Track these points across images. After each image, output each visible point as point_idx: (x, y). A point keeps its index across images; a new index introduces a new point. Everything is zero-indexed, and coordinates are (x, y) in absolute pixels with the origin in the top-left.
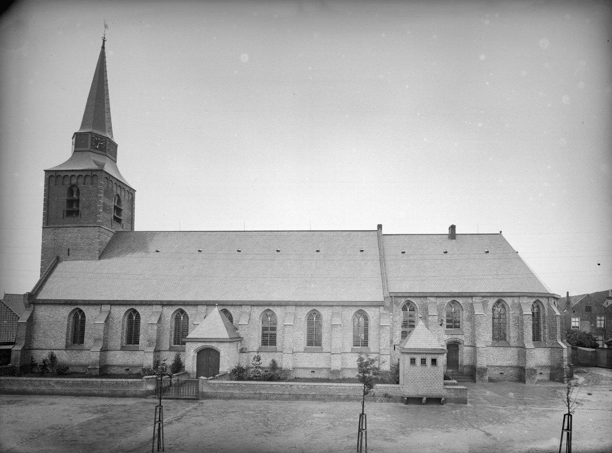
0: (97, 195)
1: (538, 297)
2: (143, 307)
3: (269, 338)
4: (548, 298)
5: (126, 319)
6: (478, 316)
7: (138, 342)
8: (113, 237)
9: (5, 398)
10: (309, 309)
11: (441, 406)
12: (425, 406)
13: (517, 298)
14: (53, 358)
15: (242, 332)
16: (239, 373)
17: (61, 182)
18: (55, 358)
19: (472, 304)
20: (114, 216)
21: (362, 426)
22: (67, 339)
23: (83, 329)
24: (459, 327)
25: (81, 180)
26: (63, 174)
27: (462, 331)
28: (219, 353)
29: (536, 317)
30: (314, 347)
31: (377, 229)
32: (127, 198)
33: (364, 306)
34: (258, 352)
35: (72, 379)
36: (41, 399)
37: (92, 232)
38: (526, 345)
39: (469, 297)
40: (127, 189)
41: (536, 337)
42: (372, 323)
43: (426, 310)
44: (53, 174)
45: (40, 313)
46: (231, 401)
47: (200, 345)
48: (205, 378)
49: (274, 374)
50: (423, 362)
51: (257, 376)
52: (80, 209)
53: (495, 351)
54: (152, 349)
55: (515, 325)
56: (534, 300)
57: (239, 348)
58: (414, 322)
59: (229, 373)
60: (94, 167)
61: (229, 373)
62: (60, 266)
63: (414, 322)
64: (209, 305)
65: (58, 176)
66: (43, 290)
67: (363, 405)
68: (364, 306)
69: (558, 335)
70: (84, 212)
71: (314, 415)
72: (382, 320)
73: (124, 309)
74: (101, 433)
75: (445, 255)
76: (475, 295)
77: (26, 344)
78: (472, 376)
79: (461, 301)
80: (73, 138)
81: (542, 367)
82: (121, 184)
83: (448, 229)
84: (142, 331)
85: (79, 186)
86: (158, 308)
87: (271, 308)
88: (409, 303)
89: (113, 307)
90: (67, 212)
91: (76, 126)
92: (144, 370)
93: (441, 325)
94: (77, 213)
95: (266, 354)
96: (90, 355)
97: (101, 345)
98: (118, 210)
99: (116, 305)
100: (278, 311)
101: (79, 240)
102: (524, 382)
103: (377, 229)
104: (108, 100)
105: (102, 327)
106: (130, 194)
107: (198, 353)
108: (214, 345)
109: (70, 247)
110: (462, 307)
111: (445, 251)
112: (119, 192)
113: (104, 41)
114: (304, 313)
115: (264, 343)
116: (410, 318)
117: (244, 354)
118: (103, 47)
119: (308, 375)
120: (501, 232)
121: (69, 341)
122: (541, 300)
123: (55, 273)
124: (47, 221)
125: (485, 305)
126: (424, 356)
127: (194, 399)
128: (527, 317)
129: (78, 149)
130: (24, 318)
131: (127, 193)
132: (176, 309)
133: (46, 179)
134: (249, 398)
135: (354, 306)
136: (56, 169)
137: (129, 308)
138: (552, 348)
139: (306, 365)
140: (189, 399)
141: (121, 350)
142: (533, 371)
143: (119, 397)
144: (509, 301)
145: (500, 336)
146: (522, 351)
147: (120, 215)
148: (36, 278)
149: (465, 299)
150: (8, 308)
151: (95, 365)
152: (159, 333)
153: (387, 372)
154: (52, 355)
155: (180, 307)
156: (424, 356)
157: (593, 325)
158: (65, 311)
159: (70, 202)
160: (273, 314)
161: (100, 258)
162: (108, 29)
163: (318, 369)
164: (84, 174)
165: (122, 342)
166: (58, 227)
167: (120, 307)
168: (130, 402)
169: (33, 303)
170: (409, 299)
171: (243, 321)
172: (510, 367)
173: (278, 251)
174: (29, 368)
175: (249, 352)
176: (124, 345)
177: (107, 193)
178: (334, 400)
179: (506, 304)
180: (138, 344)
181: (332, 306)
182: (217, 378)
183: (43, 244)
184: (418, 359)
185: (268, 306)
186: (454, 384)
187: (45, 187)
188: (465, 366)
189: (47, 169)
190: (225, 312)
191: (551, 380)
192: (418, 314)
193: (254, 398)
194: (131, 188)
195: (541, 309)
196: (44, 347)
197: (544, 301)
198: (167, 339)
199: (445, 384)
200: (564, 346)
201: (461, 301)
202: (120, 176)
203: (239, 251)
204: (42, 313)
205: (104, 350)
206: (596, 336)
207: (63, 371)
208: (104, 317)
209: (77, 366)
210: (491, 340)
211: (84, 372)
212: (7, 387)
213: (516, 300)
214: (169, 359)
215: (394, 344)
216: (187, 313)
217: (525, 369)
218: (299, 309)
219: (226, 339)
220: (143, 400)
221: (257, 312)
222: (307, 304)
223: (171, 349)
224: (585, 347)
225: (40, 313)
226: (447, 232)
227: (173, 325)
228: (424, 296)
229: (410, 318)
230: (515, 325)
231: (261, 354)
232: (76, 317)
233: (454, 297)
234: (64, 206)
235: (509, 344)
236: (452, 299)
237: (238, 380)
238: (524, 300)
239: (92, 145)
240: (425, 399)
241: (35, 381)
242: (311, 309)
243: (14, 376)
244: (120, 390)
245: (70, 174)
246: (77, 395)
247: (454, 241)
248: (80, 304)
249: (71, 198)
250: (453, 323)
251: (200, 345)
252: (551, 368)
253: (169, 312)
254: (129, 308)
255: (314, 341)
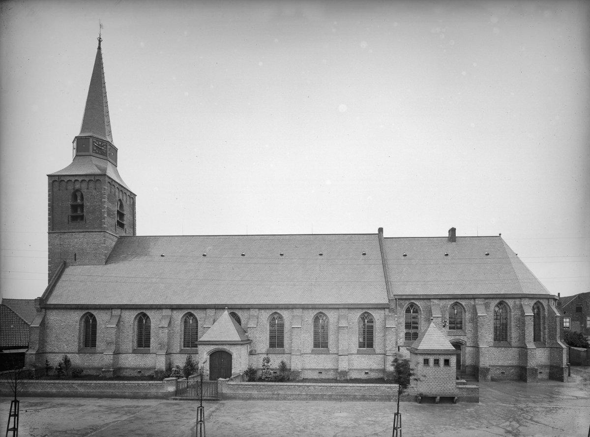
0: (101, 200)
1: (539, 298)
2: (153, 311)
3: (277, 341)
4: (548, 299)
5: (136, 323)
6: (481, 318)
7: (149, 345)
8: (118, 241)
9: (2, 398)
10: (316, 312)
11: (454, 405)
12: (438, 405)
13: (519, 300)
14: (67, 361)
15: (250, 334)
16: (251, 375)
17: (64, 187)
18: (69, 361)
19: (474, 306)
20: (118, 221)
21: (397, 424)
22: (79, 343)
23: (148, 334)
24: (461, 328)
25: (84, 185)
26: (66, 179)
27: (465, 333)
28: (231, 355)
29: (537, 317)
30: (321, 349)
31: (377, 233)
32: (128, 203)
33: (369, 308)
34: (267, 354)
35: (95, 382)
36: (66, 401)
37: (97, 237)
38: (527, 345)
39: (471, 299)
40: (128, 194)
41: (537, 339)
42: (377, 326)
43: (430, 311)
44: (56, 179)
45: (52, 318)
46: (251, 402)
47: (212, 348)
48: (224, 379)
49: (284, 375)
50: (437, 362)
51: (268, 378)
52: (85, 214)
53: (496, 352)
54: (164, 352)
55: (516, 326)
56: (535, 301)
57: (249, 350)
58: (417, 323)
59: (241, 374)
60: (97, 171)
61: (241, 374)
62: (68, 271)
63: (417, 323)
64: (218, 309)
65: (62, 180)
66: (53, 294)
67: (398, 405)
68: (369, 308)
69: (558, 335)
70: (89, 217)
71: (336, 415)
72: (387, 322)
73: (134, 314)
74: (139, 433)
75: (445, 257)
76: (478, 297)
77: (39, 347)
78: (474, 375)
79: (463, 303)
80: (73, 142)
81: (542, 366)
82: (126, 191)
83: (448, 231)
84: (152, 334)
85: (82, 191)
86: (167, 312)
87: (278, 311)
88: (412, 305)
89: (124, 311)
90: (72, 217)
91: (77, 132)
92: (157, 372)
93: (444, 326)
94: (82, 218)
95: (274, 355)
96: (102, 358)
97: (113, 347)
98: (121, 215)
99: (126, 309)
100: (285, 314)
101: (85, 245)
102: (525, 381)
103: (377, 233)
104: (107, 103)
105: (114, 331)
106: (131, 199)
107: (211, 356)
108: (227, 348)
109: (77, 252)
110: (464, 308)
111: (446, 253)
112: (121, 198)
113: (100, 41)
114: (310, 315)
115: (272, 345)
116: (413, 320)
117: (254, 356)
118: (99, 48)
119: (315, 376)
120: (500, 234)
121: (81, 344)
122: (541, 301)
123: (63, 278)
124: (53, 226)
125: (487, 306)
126: (437, 357)
127: (214, 400)
128: (529, 318)
129: (80, 154)
130: (36, 323)
131: (128, 198)
132: (84, 313)
133: (49, 184)
134: (267, 399)
135: (360, 308)
136: (57, 174)
137: (139, 312)
138: (551, 348)
139: (314, 366)
140: (208, 400)
141: (358, 354)
142: (534, 371)
143: (142, 399)
144: (510, 303)
145: (501, 336)
146: (523, 351)
147: (123, 220)
148: (44, 285)
149: (468, 301)
150: (13, 312)
151: (109, 367)
152: (170, 336)
153: (392, 373)
154: (66, 359)
155: (189, 311)
156: (437, 357)
157: (583, 326)
158: (77, 316)
159: (74, 208)
160: (281, 317)
161: (106, 263)
162: (103, 28)
163: (325, 370)
164: (87, 179)
165: (180, 346)
166: (65, 233)
167: (130, 311)
168: (153, 403)
169: (45, 308)
170: (413, 301)
171: (252, 324)
172: (511, 366)
173: (282, 255)
174: (45, 372)
175: (258, 354)
176: (135, 348)
177: (111, 198)
178: (350, 400)
179: (508, 306)
180: (149, 347)
181: (338, 308)
182: (232, 380)
183: (50, 250)
184: (431, 360)
185: (275, 310)
186: (464, 384)
187: (49, 192)
188: (467, 366)
189: (50, 173)
190: (234, 315)
191: (550, 379)
192: (422, 317)
193: (272, 399)
194: (131, 193)
195: (541, 310)
196: (57, 350)
197: (544, 303)
198: (177, 343)
199: (457, 384)
200: (564, 346)
201: (463, 303)
202: (121, 180)
203: (243, 255)
204: (54, 317)
205: (117, 353)
206: (587, 336)
207: (78, 374)
208: (115, 320)
209: (90, 369)
210: (492, 341)
211: (98, 375)
212: (31, 390)
213: (518, 302)
214: (180, 361)
215: (399, 345)
216: (197, 316)
217: (526, 369)
218: (306, 312)
219: (238, 341)
220: (165, 401)
221: (265, 316)
222: (313, 307)
223: (181, 352)
224: (576, 346)
225: (52, 318)
226: (377, 232)
227: (183, 328)
228: (428, 298)
229: (413, 320)
230: (516, 326)
231: (270, 356)
232: (87, 322)
233: (457, 299)
234: (70, 212)
235: (510, 343)
236: (455, 301)
237: (249, 381)
238: (525, 302)
239: (93, 150)
240: (438, 398)
241: (59, 383)
242: (317, 311)
243: (30, 379)
244: (143, 392)
245: (73, 179)
246: (100, 397)
247: (454, 243)
248: (91, 309)
249: (75, 203)
250: (455, 324)
251: (212, 348)
252: (551, 367)
253: (179, 316)
254: (139, 312)
255: (321, 343)
